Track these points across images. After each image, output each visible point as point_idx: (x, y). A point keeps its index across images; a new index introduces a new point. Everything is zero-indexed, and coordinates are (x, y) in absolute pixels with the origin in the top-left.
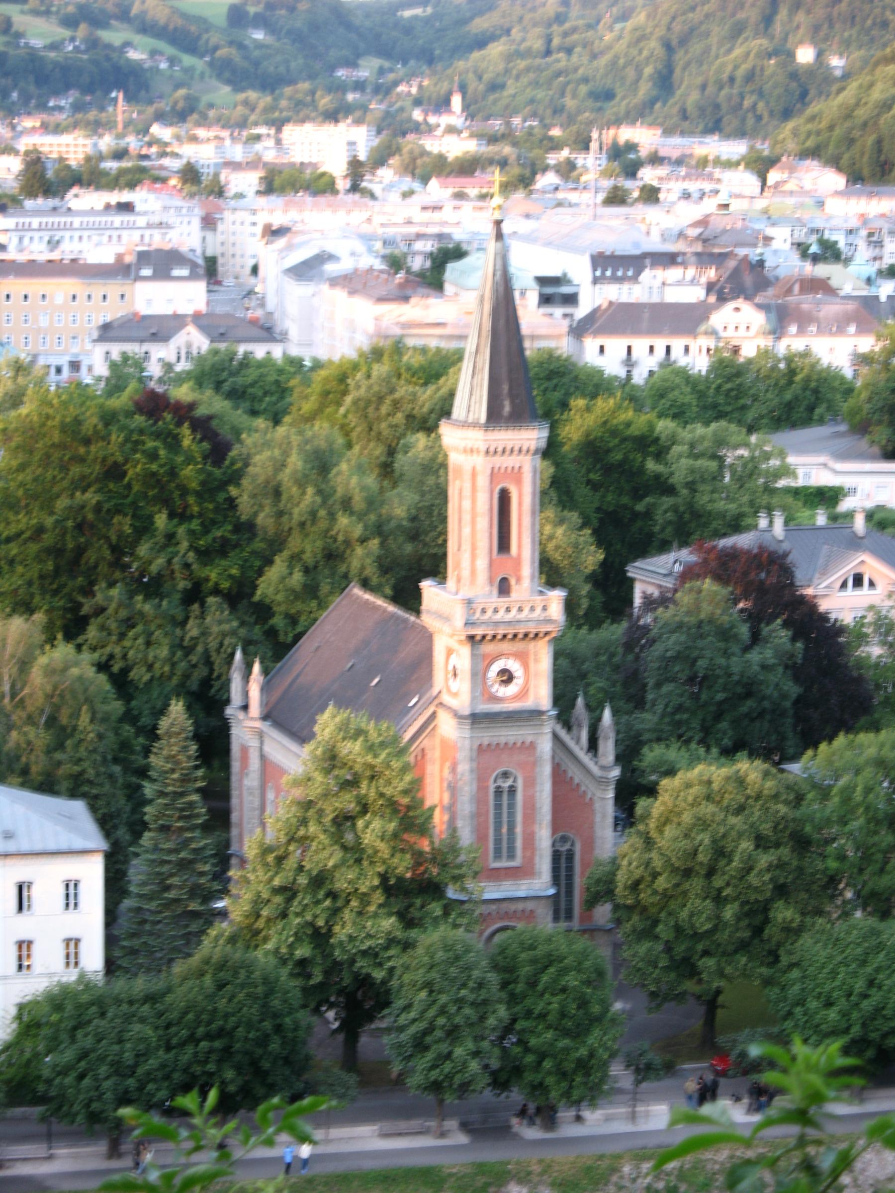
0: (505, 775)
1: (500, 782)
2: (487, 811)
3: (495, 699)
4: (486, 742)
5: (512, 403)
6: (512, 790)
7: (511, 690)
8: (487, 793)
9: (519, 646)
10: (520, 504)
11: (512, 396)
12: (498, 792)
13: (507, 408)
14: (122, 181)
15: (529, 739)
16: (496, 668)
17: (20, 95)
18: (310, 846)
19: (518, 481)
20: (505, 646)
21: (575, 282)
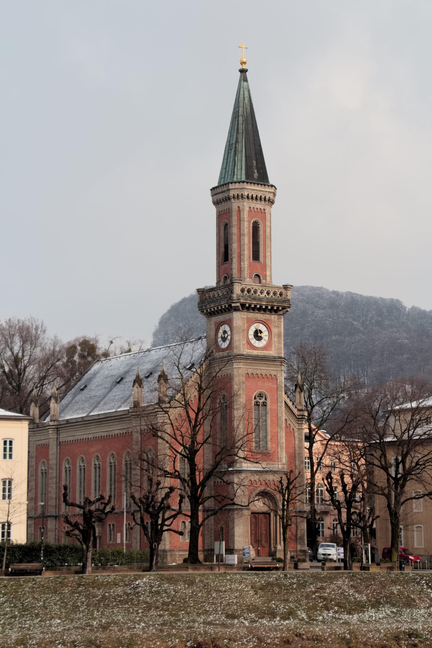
0: (260, 395)
3: (255, 348)
7: (260, 344)
13: (256, 175)
15: (273, 373)
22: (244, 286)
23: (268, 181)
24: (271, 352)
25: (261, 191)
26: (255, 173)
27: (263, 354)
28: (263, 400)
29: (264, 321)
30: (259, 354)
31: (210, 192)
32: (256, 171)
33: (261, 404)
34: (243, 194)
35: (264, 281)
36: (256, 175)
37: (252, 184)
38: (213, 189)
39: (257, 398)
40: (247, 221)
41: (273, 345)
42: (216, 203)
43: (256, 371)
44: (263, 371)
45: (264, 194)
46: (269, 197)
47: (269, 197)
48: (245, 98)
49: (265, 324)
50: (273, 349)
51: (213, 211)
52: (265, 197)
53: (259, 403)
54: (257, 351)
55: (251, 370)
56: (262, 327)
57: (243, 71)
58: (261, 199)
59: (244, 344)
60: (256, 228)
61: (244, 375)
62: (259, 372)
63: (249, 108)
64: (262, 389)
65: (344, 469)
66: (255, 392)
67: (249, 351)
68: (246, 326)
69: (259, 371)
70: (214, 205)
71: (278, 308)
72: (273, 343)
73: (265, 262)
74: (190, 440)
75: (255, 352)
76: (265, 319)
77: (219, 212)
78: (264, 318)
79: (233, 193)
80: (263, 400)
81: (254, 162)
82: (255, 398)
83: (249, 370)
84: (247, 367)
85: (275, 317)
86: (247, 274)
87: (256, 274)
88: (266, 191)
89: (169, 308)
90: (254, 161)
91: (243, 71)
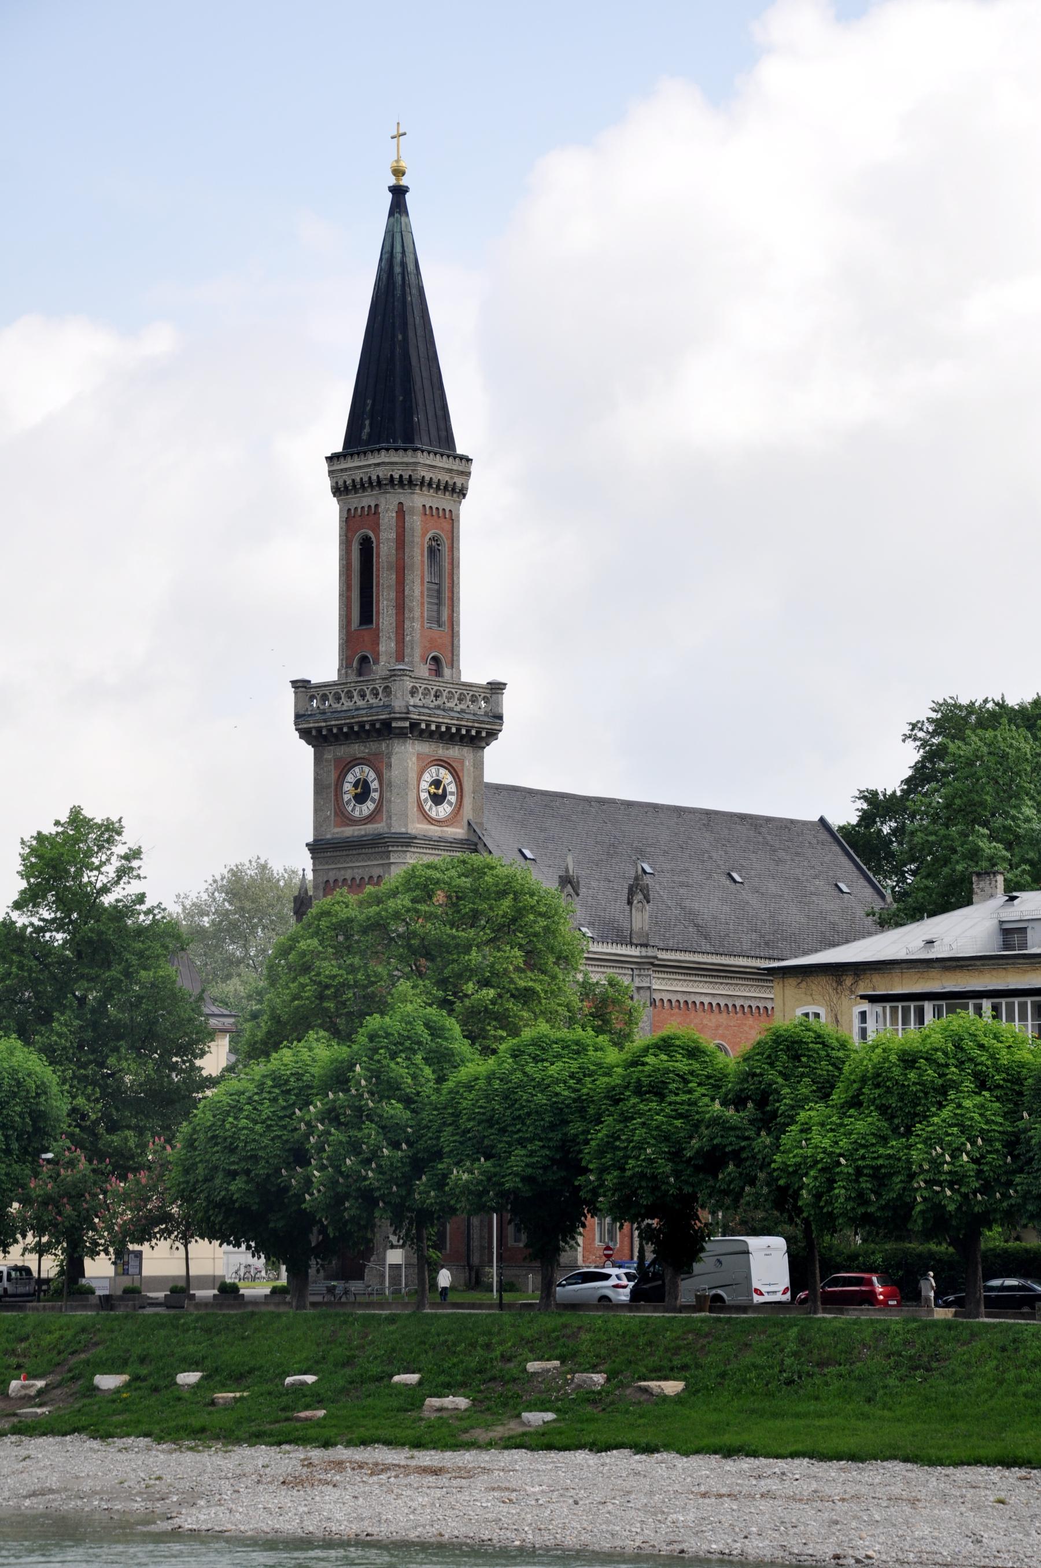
3: (431, 821)
7: (443, 811)
19: (376, 528)
20: (358, 749)
23: (454, 448)
24: (379, 825)
25: (359, 468)
27: (363, 833)
30: (356, 833)
31: (324, 467)
34: (413, 478)
35: (447, 672)
37: (383, 452)
38: (331, 459)
42: (338, 491)
43: (349, 871)
44: (356, 871)
46: (378, 476)
47: (378, 476)
51: (330, 510)
52: (370, 478)
54: (352, 828)
57: (399, 193)
58: (438, 486)
59: (328, 817)
60: (433, 552)
62: (348, 874)
67: (337, 830)
70: (334, 494)
71: (478, 733)
74: (274, 1055)
75: (349, 831)
77: (349, 510)
79: (423, 474)
83: (331, 873)
84: (326, 867)
88: (370, 465)
89: (303, 742)
91: (399, 193)
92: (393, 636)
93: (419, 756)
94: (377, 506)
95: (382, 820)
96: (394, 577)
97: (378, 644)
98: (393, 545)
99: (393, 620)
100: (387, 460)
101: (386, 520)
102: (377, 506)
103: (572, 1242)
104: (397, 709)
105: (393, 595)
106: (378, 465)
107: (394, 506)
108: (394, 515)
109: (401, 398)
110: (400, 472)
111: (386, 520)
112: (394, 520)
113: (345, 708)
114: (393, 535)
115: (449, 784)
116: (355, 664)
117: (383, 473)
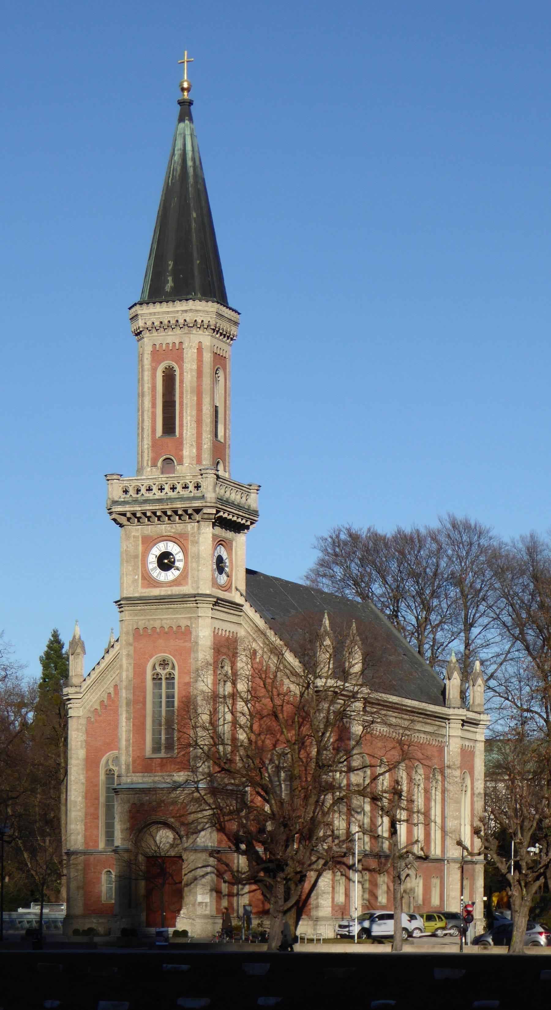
0: (164, 663)
1: (159, 670)
2: (145, 698)
3: (156, 584)
4: (141, 625)
5: (174, 281)
6: (170, 678)
7: (172, 575)
8: (144, 681)
9: (178, 527)
10: (182, 382)
11: (175, 274)
12: (157, 678)
13: (169, 285)
14: (373, 826)
15: (184, 623)
16: (157, 550)
17: (165, 559)
18: (127, 660)
19: (180, 359)
20: (164, 528)
21: (231, 301)
22: (126, 484)
25: (168, 313)
26: (168, 282)
27: (169, 593)
28: (168, 670)
29: (175, 536)
32: (170, 279)
33: (163, 678)
36: (169, 285)
39: (157, 667)
40: (148, 370)
41: (190, 576)
45: (175, 317)
48: (176, 152)
49: (176, 541)
50: (190, 581)
52: (177, 321)
53: (166, 675)
55: (143, 622)
56: (173, 548)
59: (136, 580)
61: (131, 633)
62: (157, 624)
63: (179, 168)
64: (165, 653)
65: (317, 763)
66: (151, 658)
67: (144, 590)
68: (140, 548)
69: (159, 622)
72: (190, 570)
73: (181, 434)
75: (156, 592)
76: (175, 533)
78: (173, 531)
80: (168, 670)
81: (171, 263)
82: (154, 668)
85: (193, 527)
86: (148, 460)
87: (164, 457)
88: (178, 311)
90: (170, 262)
92: (194, 444)
93: (214, 536)
94: (181, 343)
95: (187, 584)
96: (195, 398)
97: (182, 450)
98: (195, 374)
99: (194, 432)
100: (193, 308)
101: (189, 355)
102: (181, 343)
103: (521, 950)
104: (209, 500)
105: (194, 413)
106: (186, 311)
107: (195, 345)
108: (196, 351)
109: (198, 262)
110: (202, 319)
111: (189, 355)
112: (196, 354)
113: (156, 497)
114: (195, 367)
115: (179, 561)
116: (159, 464)
117: (189, 317)
